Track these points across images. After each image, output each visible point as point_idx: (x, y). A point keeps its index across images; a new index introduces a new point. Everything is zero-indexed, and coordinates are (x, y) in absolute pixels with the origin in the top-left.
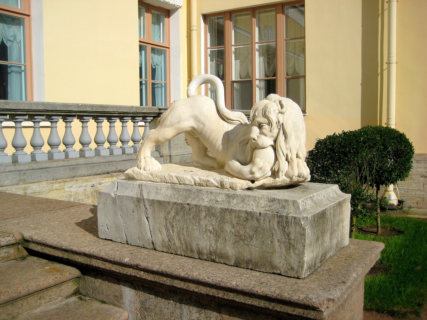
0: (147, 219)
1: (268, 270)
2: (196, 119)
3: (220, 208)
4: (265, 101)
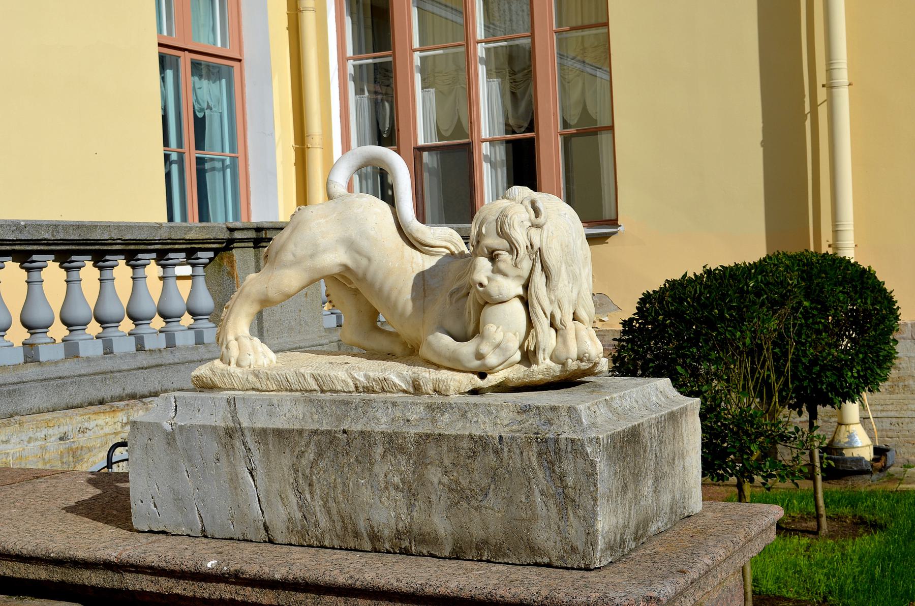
0: (251, 473)
1: (523, 559)
2: (351, 246)
4: (503, 203)
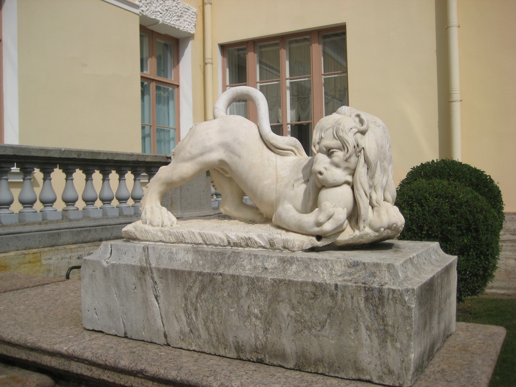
0: (156, 298)
3: (271, 279)
